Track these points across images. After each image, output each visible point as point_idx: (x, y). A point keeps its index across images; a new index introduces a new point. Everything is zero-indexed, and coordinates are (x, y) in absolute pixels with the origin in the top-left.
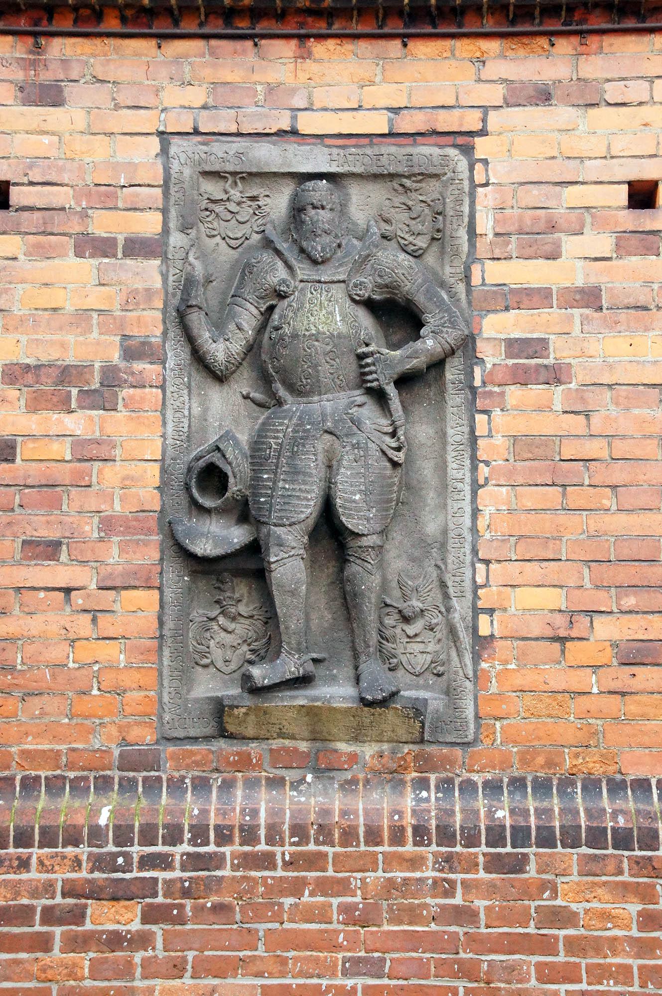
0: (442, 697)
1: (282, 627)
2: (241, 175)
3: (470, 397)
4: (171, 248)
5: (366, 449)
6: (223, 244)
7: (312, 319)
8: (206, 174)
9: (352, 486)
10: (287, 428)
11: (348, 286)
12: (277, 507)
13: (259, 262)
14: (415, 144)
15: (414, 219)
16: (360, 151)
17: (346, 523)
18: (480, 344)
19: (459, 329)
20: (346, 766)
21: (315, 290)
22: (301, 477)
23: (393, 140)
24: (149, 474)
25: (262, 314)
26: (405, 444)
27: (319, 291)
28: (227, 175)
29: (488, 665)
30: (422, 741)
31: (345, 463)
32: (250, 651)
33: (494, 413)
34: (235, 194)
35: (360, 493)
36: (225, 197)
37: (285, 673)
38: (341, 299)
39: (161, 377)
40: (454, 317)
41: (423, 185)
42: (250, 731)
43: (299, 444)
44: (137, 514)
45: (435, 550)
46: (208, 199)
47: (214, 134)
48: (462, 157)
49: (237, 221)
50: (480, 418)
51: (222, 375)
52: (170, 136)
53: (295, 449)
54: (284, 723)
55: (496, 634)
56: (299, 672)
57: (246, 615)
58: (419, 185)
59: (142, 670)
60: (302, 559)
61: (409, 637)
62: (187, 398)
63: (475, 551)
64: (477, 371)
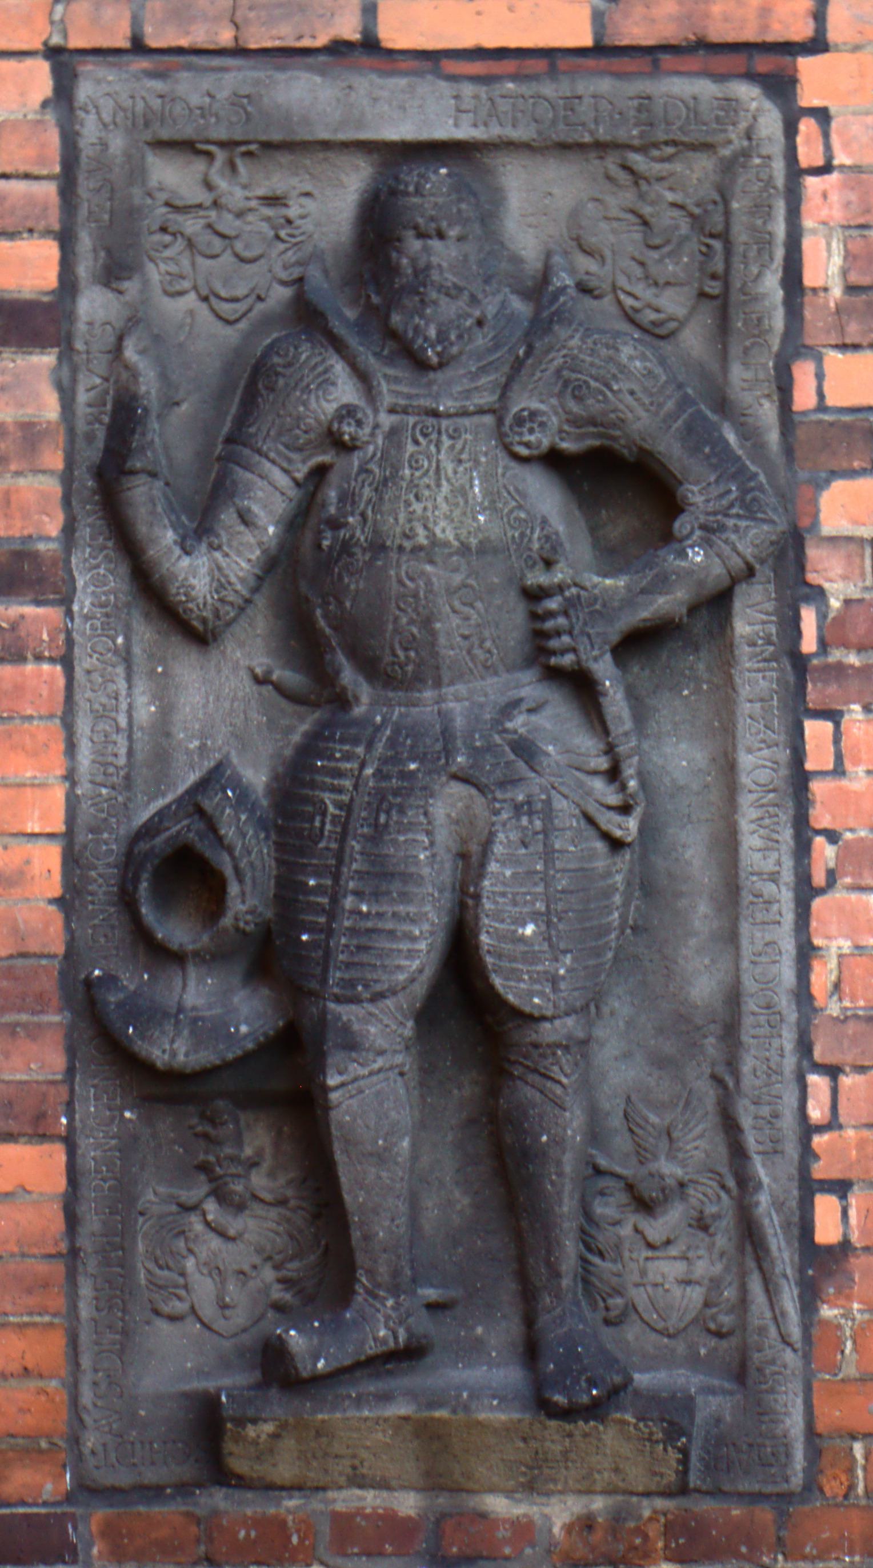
0: (727, 1385)
1: (356, 1235)
2: (243, 149)
3: (791, 678)
4: (81, 327)
5: (548, 812)
6: (203, 310)
7: (417, 507)
8: (161, 145)
9: (515, 904)
10: (363, 765)
11: (500, 421)
12: (341, 957)
13: (289, 365)
14: (656, 70)
15: (656, 248)
16: (525, 89)
17: (501, 990)
18: (813, 552)
19: (764, 521)
20: (507, 1551)
21: (425, 435)
22: (396, 886)
23: (603, 62)
24: (37, 868)
25: (297, 484)
26: (641, 796)
27: (434, 436)
28: (212, 148)
29: (836, 1312)
30: (683, 1490)
31: (498, 849)
32: (280, 1281)
33: (847, 717)
34: (234, 194)
35: (535, 922)
36: (203, 197)
37: (363, 1343)
38: (486, 454)
39: (62, 637)
40: (752, 489)
41: (678, 167)
42: (284, 1471)
43: (391, 806)
44: (11, 962)
45: (711, 1040)
46: (167, 204)
47: (180, 51)
48: (768, 105)
49: (237, 255)
50: (816, 730)
51: (206, 630)
52: (77, 58)
53: (382, 819)
54: (364, 1454)
55: (855, 1237)
56: (396, 1338)
57: (267, 1197)
58: (667, 166)
59: (30, 1332)
60: (402, 1074)
61: (650, 1246)
62: (122, 685)
63: (805, 1046)
64: (809, 618)
